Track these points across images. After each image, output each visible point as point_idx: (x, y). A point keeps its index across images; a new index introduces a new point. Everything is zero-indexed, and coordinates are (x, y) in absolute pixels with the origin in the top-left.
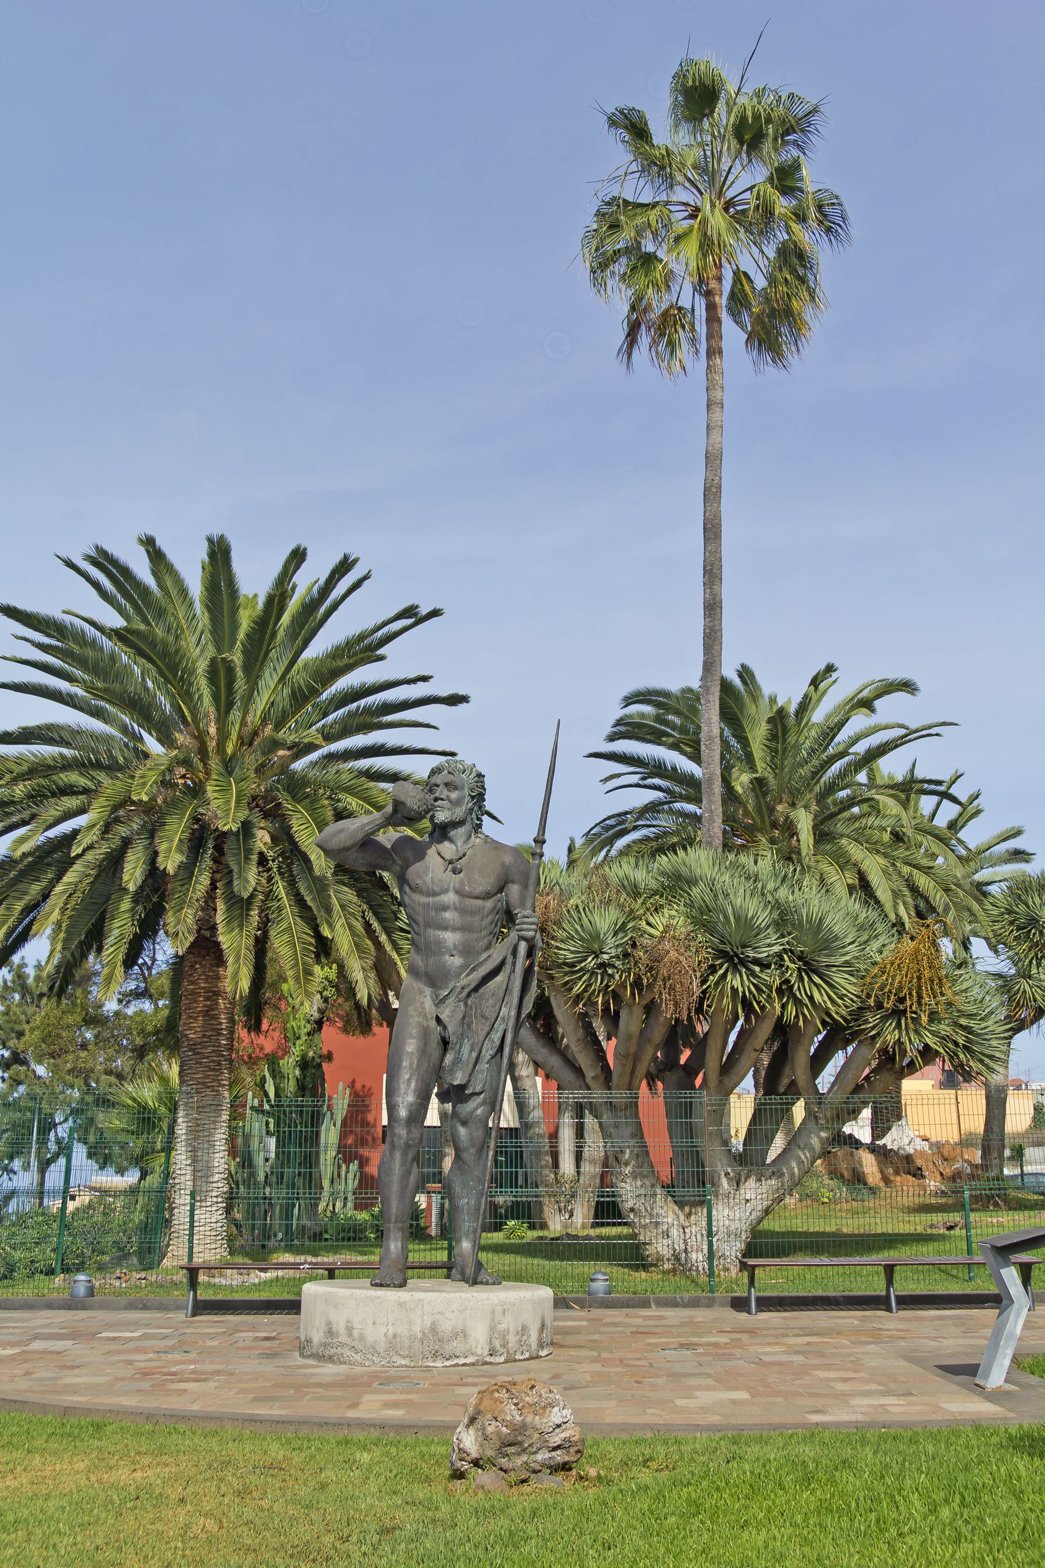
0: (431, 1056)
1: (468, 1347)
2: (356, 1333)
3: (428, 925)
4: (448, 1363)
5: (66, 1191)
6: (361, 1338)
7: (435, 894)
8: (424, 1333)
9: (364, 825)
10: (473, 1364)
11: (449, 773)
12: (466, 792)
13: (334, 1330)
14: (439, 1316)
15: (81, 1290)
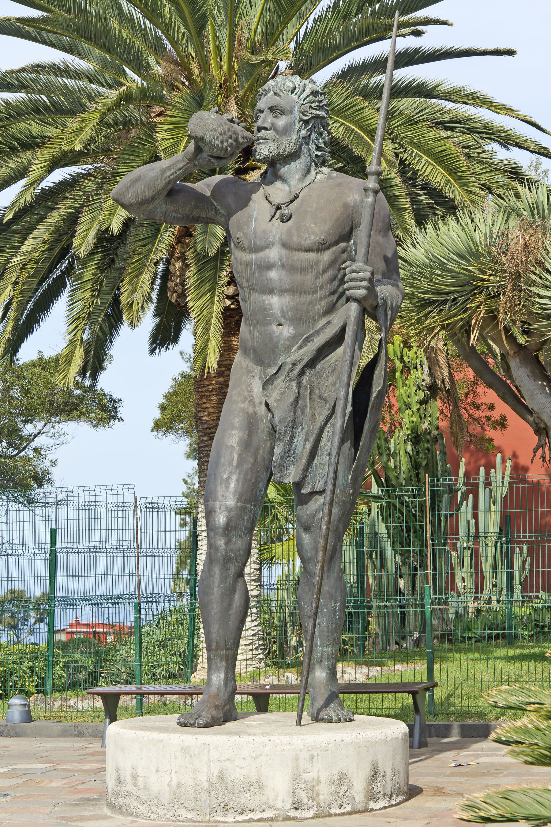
0: (258, 449)
1: (264, 799)
2: (140, 781)
3: (252, 289)
4: (240, 818)
5: (139, 594)
6: (146, 787)
7: (257, 249)
8: (211, 783)
9: (163, 171)
10: (272, 819)
11: (275, 94)
12: (297, 115)
13: (122, 778)
14: (227, 763)
15: (16, 714)
